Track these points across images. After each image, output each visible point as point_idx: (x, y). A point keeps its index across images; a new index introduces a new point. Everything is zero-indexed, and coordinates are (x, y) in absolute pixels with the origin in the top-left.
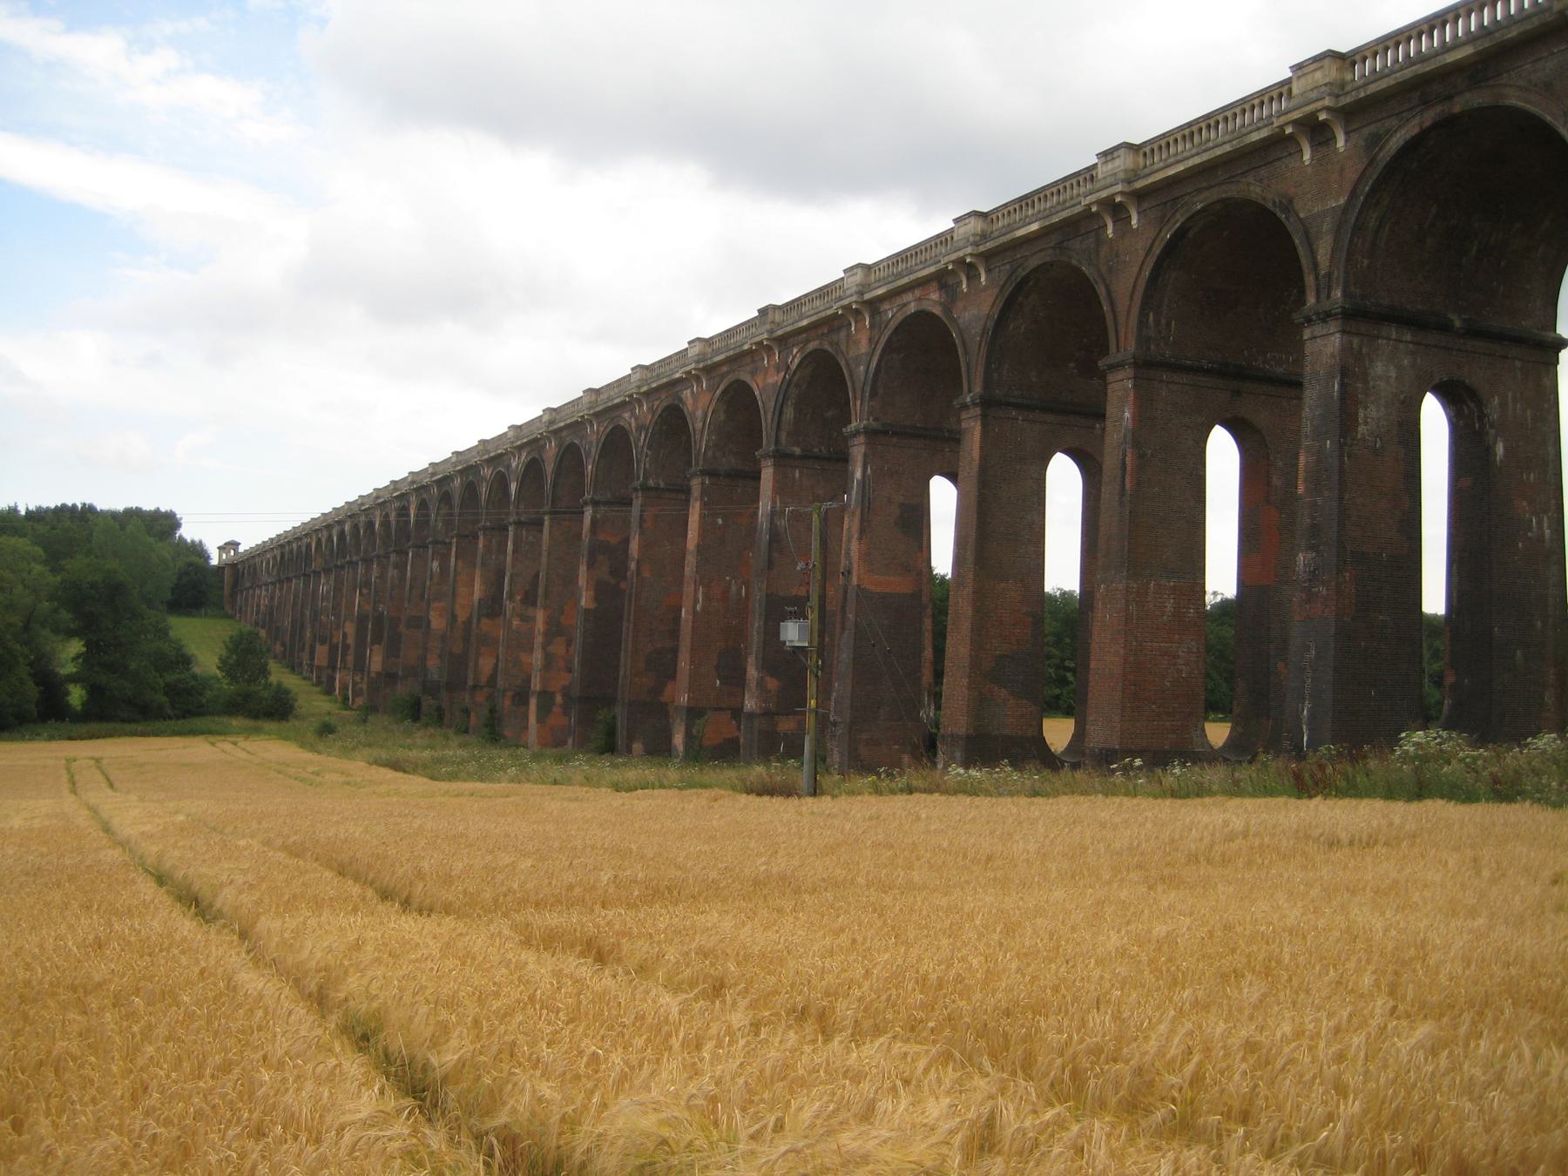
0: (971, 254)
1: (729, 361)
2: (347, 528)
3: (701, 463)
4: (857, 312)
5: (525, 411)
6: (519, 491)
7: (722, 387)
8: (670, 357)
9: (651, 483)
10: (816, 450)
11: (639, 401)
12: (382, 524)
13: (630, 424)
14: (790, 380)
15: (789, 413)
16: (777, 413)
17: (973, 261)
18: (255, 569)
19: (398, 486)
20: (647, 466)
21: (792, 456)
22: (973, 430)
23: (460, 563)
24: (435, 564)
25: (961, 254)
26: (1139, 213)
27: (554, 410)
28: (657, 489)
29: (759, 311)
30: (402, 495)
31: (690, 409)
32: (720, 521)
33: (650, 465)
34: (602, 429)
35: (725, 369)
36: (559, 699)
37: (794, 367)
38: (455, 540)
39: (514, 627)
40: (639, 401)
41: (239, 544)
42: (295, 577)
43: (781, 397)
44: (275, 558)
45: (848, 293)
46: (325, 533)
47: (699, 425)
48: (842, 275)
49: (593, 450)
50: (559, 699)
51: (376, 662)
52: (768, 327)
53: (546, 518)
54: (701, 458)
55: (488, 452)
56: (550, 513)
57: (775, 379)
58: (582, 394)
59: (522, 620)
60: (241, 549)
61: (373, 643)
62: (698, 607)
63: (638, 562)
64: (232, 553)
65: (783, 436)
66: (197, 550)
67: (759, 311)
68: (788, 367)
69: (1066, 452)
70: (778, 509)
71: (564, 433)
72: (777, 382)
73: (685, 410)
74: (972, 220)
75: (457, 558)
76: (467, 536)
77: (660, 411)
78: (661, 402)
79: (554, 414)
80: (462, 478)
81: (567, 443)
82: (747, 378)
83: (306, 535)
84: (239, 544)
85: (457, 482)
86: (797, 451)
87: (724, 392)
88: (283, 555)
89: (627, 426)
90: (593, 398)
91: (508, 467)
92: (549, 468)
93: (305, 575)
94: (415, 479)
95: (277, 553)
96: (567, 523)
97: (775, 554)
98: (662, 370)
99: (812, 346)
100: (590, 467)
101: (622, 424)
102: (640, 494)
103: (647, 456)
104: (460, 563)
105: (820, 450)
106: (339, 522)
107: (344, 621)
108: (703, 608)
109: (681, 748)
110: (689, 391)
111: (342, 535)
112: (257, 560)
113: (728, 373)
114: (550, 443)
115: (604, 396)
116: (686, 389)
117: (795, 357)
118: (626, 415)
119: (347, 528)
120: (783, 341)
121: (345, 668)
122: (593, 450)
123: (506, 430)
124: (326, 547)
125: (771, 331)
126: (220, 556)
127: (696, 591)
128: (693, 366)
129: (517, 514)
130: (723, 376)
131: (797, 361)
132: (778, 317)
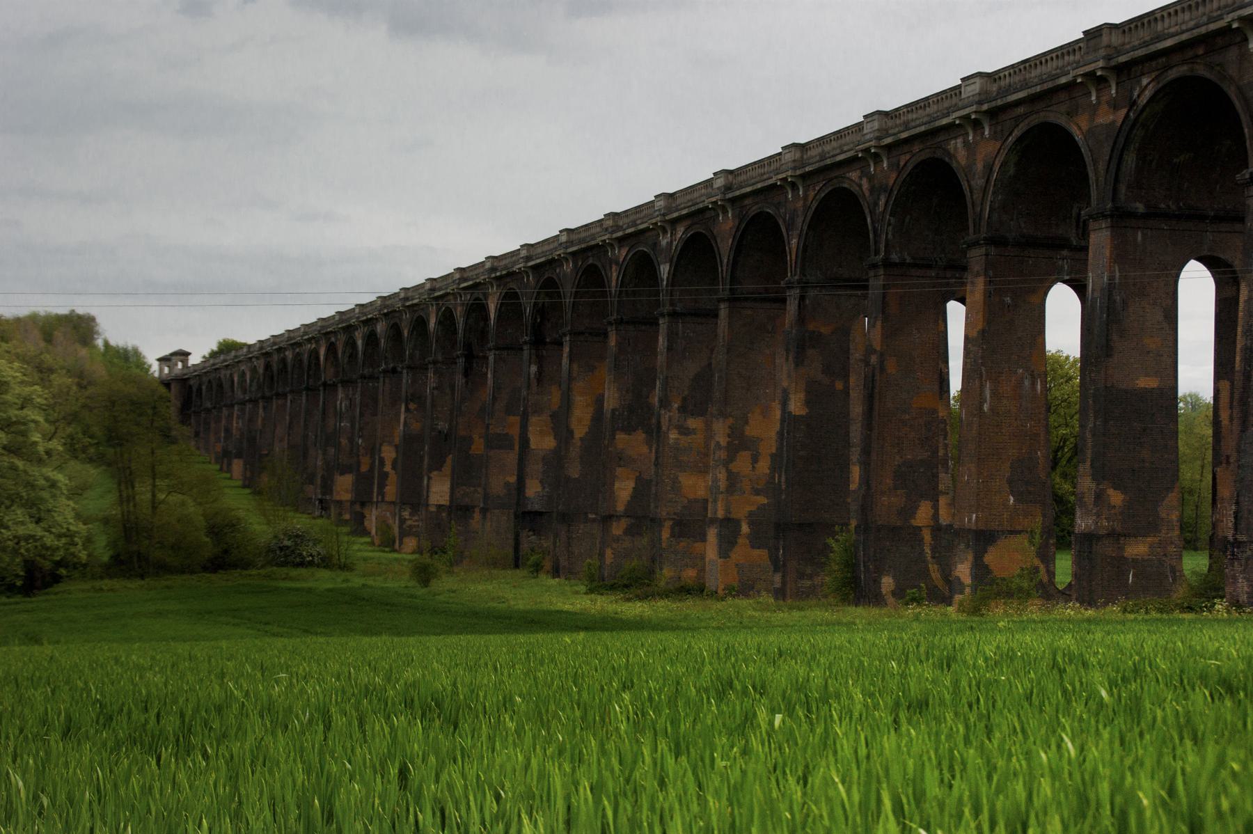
0: (791, 176)
1: (1032, 99)
2: (380, 328)
3: (984, 229)
4: (876, 156)
5: (503, 241)
6: (674, 275)
7: (1017, 133)
8: (927, 98)
9: (895, 257)
10: (1163, 206)
11: (876, 157)
12: (439, 323)
13: (860, 186)
14: (1136, 119)
15: (1130, 160)
16: (1115, 161)
17: (1104, 74)
18: (220, 386)
19: (252, 350)
20: (890, 236)
21: (1133, 215)
22: (1100, 239)
23: (575, 367)
24: (534, 369)
25: (867, 145)
26: (803, 187)
27: (731, 172)
28: (902, 264)
29: (1084, 32)
30: (476, 286)
31: (963, 162)
32: (1008, 300)
33: (893, 235)
34: (812, 194)
35: (1021, 110)
36: (745, 528)
37: (1143, 100)
38: (568, 338)
39: (671, 441)
40: (876, 157)
41: (189, 354)
42: (292, 392)
43: (1122, 140)
44: (254, 370)
45: (868, 137)
46: (342, 338)
47: (979, 182)
48: (781, 150)
49: (799, 220)
50: (745, 528)
51: (439, 491)
52: (1102, 52)
53: (722, 306)
54: (984, 223)
55: (618, 228)
56: (729, 300)
57: (1110, 117)
58: (603, 217)
59: (680, 433)
60: (195, 360)
61: (430, 470)
62: (986, 407)
63: (882, 355)
64: (180, 365)
65: (1123, 189)
66: (128, 359)
67: (1084, 32)
68: (1134, 103)
69: (1199, 259)
70: (1117, 281)
71: (747, 202)
72: (1114, 122)
73: (954, 165)
74: (977, 80)
75: (571, 361)
76: (582, 333)
77: (910, 167)
78: (919, 153)
79: (730, 177)
80: (575, 263)
81: (752, 213)
82: (1062, 121)
83: (309, 340)
84: (189, 354)
85: (568, 267)
86: (1140, 208)
87: (1019, 140)
88: (268, 367)
89: (855, 189)
90: (798, 155)
91: (655, 245)
92: (725, 247)
93: (308, 389)
94: (307, 330)
95: (260, 365)
96: (749, 312)
97: (1115, 337)
98: (910, 116)
99: (1173, 74)
100: (794, 241)
101: (846, 185)
102: (881, 272)
103: (889, 224)
104: (575, 367)
105: (1168, 206)
106: (367, 322)
107: (381, 445)
108: (992, 409)
109: (967, 581)
110: (960, 141)
111: (371, 339)
112: (224, 374)
113: (1026, 115)
114: (528, 277)
115: (814, 152)
116: (955, 138)
117: (1146, 87)
118: (854, 175)
119: (380, 328)
120: (1125, 71)
121: (383, 501)
122: (799, 220)
123: (424, 281)
124: (344, 352)
125: (1108, 58)
126: (161, 370)
127: (982, 387)
128: (974, 108)
129: (672, 304)
130: (1017, 120)
131: (1148, 94)
132: (1116, 39)
